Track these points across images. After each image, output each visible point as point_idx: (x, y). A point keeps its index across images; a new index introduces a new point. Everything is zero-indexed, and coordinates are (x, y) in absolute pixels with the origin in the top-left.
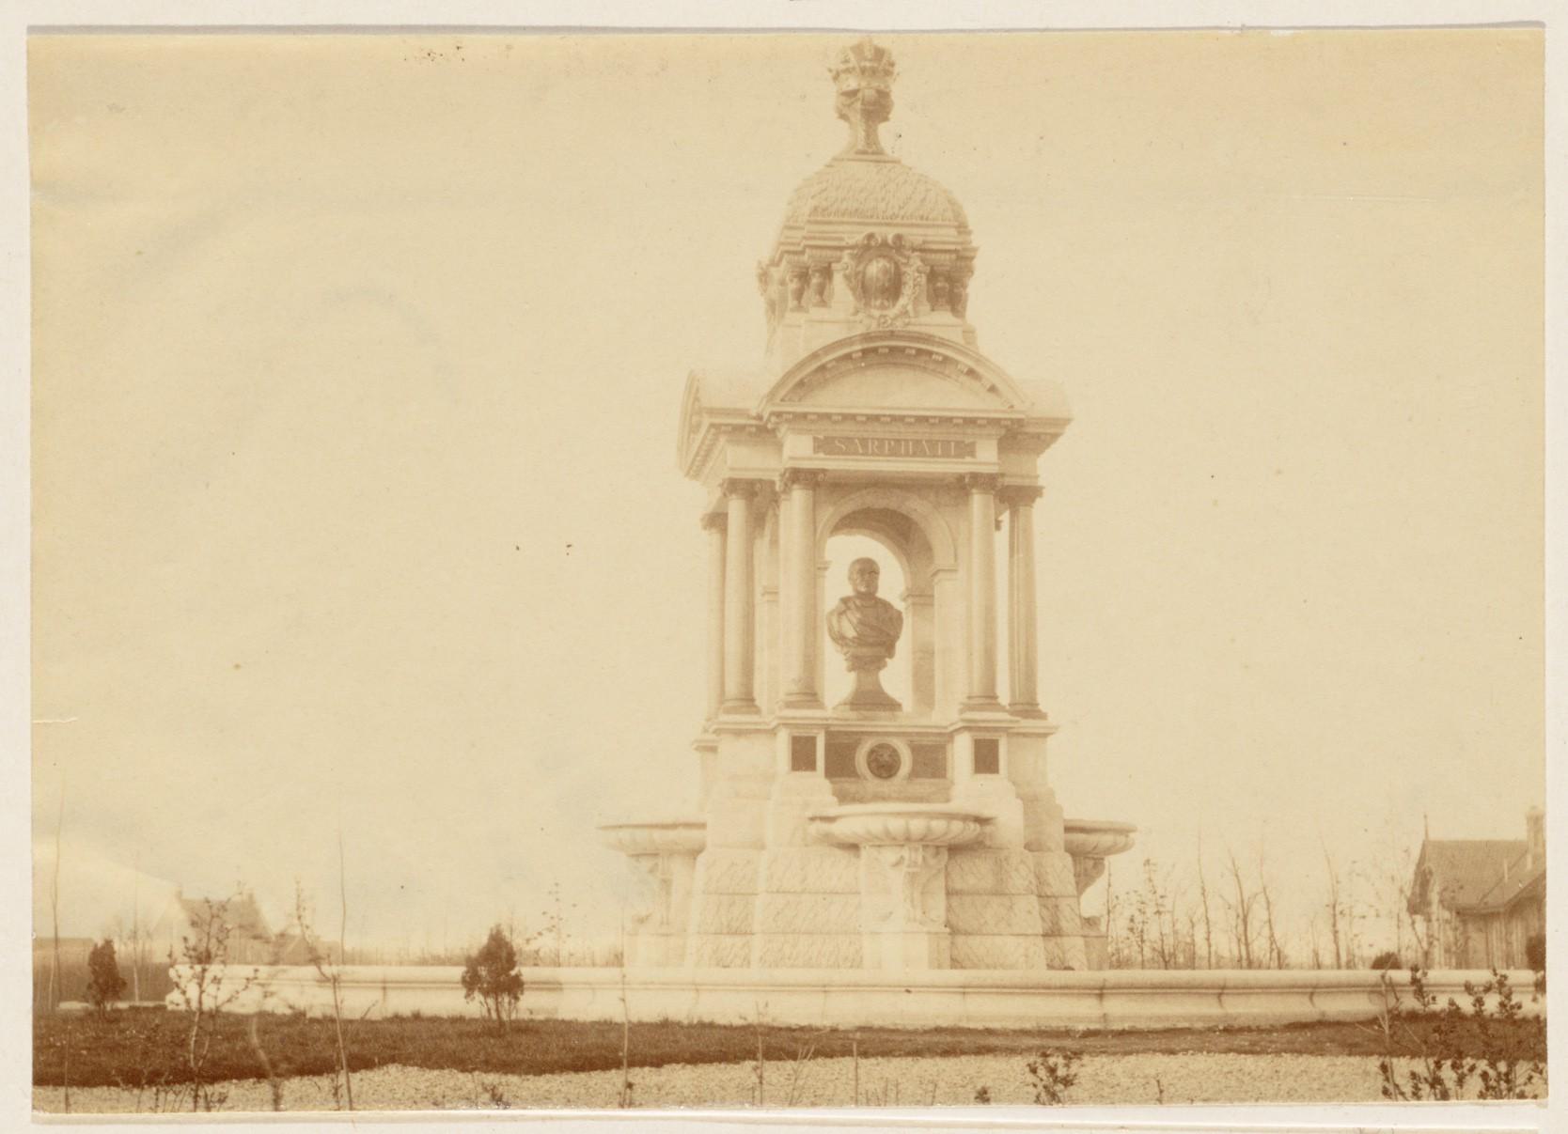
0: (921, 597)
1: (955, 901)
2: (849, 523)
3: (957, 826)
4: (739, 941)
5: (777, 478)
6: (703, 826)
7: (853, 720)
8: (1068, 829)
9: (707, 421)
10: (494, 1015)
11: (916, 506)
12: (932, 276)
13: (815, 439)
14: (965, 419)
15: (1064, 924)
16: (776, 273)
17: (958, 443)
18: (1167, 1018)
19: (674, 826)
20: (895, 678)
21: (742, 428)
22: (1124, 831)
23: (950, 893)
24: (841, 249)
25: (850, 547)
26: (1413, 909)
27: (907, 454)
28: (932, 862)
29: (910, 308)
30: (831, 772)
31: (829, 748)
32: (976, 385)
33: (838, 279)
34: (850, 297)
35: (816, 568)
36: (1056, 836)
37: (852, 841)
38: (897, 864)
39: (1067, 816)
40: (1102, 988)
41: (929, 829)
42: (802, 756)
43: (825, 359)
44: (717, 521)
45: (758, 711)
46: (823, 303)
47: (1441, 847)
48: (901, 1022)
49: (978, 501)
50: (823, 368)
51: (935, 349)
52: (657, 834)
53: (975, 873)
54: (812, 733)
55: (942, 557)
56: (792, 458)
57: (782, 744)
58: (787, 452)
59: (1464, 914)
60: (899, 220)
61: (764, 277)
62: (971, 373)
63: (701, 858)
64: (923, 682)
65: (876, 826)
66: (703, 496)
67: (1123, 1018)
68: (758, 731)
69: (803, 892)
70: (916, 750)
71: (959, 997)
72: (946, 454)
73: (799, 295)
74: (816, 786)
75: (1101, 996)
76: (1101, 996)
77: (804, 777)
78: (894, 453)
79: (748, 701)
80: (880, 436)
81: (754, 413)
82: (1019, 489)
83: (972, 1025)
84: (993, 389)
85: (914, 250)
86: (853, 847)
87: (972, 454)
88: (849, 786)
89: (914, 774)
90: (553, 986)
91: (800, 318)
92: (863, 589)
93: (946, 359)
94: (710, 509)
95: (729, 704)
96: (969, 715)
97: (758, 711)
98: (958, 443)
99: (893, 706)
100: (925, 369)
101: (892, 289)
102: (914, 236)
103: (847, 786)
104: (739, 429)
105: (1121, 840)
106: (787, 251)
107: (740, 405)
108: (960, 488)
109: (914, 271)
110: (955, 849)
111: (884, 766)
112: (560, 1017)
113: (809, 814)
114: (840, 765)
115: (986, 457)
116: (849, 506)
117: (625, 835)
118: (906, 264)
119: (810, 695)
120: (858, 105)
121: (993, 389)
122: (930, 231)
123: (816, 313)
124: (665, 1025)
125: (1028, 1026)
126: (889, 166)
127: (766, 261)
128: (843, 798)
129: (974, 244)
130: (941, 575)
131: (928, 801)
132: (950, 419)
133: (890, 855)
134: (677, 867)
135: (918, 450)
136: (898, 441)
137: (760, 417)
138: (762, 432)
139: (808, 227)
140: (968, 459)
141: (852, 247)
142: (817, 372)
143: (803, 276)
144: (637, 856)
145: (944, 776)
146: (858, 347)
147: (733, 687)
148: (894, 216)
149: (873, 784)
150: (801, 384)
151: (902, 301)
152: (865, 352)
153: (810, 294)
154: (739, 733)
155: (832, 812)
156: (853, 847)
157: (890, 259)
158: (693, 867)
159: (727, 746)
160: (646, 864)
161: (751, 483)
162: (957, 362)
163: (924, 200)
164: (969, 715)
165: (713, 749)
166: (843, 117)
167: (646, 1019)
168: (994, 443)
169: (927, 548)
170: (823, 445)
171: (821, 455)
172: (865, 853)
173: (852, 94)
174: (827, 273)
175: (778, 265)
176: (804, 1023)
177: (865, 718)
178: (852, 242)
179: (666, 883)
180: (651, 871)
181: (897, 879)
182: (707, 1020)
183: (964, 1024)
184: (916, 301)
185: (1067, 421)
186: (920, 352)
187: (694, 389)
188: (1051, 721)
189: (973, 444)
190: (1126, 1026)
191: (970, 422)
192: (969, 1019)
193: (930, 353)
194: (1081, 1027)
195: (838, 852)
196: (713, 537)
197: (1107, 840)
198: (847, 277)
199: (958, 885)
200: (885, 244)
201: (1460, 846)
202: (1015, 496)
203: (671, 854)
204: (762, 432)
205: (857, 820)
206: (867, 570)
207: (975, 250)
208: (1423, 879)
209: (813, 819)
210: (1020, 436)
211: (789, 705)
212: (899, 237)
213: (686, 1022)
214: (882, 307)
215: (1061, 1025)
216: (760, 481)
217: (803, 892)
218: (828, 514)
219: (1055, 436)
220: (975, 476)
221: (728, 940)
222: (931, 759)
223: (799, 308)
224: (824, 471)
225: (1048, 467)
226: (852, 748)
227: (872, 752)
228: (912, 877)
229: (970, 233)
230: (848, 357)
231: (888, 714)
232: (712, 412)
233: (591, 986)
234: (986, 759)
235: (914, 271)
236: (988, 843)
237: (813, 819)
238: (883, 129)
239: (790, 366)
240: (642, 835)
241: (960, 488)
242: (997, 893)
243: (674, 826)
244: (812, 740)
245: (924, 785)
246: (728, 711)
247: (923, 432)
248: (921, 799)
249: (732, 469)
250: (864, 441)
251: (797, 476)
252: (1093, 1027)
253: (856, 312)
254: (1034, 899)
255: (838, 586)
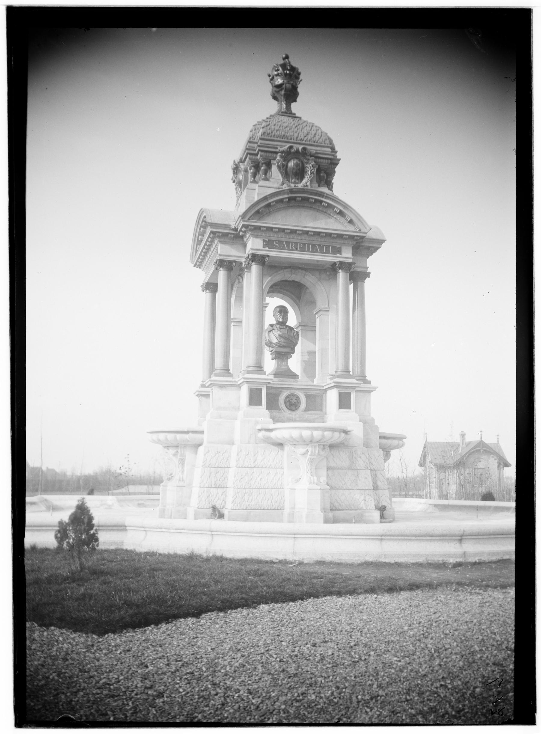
0: (308, 326)
1: (330, 473)
2: (276, 288)
3: (327, 434)
4: (220, 491)
5: (243, 261)
6: (202, 432)
7: (276, 382)
8: (380, 437)
9: (209, 230)
10: (216, 242)
11: (308, 279)
12: (319, 171)
13: (264, 241)
14: (338, 235)
15: (379, 483)
16: (242, 166)
17: (333, 247)
18: (498, 553)
19: (187, 432)
20: (294, 363)
21: (226, 235)
22: (401, 438)
23: (328, 468)
24: (276, 153)
25: (275, 302)
26: (421, 465)
27: (309, 251)
28: (322, 453)
29: (308, 184)
30: (268, 408)
31: (268, 394)
32: (342, 219)
33: (274, 168)
34: (280, 177)
35: (262, 307)
36: (375, 441)
37: (280, 442)
38: (305, 454)
39: (380, 431)
40: (462, 536)
41: (323, 436)
42: (254, 398)
43: (270, 201)
44: (211, 287)
45: (231, 376)
46: (266, 179)
47: (432, 444)
48: (346, 559)
49: (341, 276)
50: (269, 205)
51: (324, 200)
52: (178, 436)
53: (341, 459)
54: (259, 387)
55: (321, 303)
56: (252, 249)
57: (245, 391)
58: (249, 246)
59: (441, 468)
60: (304, 142)
61: (236, 170)
62: (341, 213)
63: (201, 449)
64: (309, 366)
65: (295, 434)
66: (202, 276)
67: (475, 554)
68: (232, 385)
69: (254, 467)
70: (308, 397)
71: (378, 542)
72: (327, 252)
73: (254, 175)
74: (262, 411)
75: (460, 541)
76: (460, 541)
77: (255, 409)
78: (303, 249)
79: (226, 371)
80: (296, 241)
81: (233, 227)
82: (358, 273)
83: (387, 561)
84: (351, 222)
85: (311, 156)
86: (280, 445)
87: (340, 252)
88: (276, 414)
89: (307, 409)
90: (121, 528)
91: (255, 186)
92: (281, 320)
93: (329, 206)
94: (206, 281)
95: (216, 372)
96: (336, 380)
97: (231, 376)
98: (333, 247)
99: (295, 376)
100: (318, 210)
101: (300, 174)
102: (312, 149)
103: (275, 414)
104: (225, 235)
105: (401, 442)
106: (249, 152)
107: (226, 223)
108: (332, 270)
109: (310, 167)
110: (332, 446)
111: (292, 404)
112: (125, 548)
113: (259, 427)
114: (272, 405)
115: (347, 255)
116: (278, 277)
117: (162, 436)
118: (307, 163)
119: (259, 368)
120: (283, 92)
121: (351, 222)
122: (318, 148)
123: (262, 183)
124: (191, 557)
125: (421, 560)
126: (298, 119)
127: (237, 160)
128: (275, 420)
129: (338, 157)
130: (321, 313)
131: (314, 422)
132: (330, 234)
133: (301, 450)
134: (189, 454)
135: (314, 249)
136: (304, 244)
137: (236, 229)
138: (235, 237)
139: (260, 141)
140: (338, 255)
141: (282, 152)
142: (262, 209)
143: (256, 166)
144: (168, 447)
145: (321, 410)
146: (286, 196)
147: (219, 363)
148: (301, 140)
149: (287, 413)
150: (258, 212)
151: (305, 181)
152: (290, 199)
153: (261, 175)
154: (221, 386)
155: (272, 426)
156: (280, 445)
157: (300, 160)
158: (196, 453)
159: (216, 392)
160: (172, 451)
161: (230, 262)
162: (334, 207)
163: (315, 134)
164: (336, 380)
165: (207, 396)
166: (275, 98)
167: (179, 552)
168: (351, 248)
169: (313, 303)
170: (268, 244)
171: (267, 249)
172: (287, 448)
173: (279, 86)
174: (269, 165)
175: (243, 162)
176: (281, 557)
177: (282, 381)
178: (282, 149)
179: (182, 461)
180: (174, 455)
181: (304, 463)
182: (218, 554)
183: (383, 560)
184: (311, 182)
185: (383, 241)
186: (317, 201)
187: (202, 211)
188: (373, 384)
189: (340, 248)
190: (476, 559)
191: (340, 236)
192: (385, 556)
193: (321, 202)
194: (452, 561)
195: (272, 447)
196: (207, 295)
197: (395, 442)
198: (279, 167)
199: (332, 464)
200: (297, 151)
201: (437, 443)
202: (358, 277)
203: (185, 446)
204: (235, 237)
205: (285, 430)
206: (283, 311)
207: (339, 160)
208: (424, 456)
209: (260, 430)
210: (365, 246)
211: (248, 372)
212: (304, 149)
213: (205, 555)
214: (295, 183)
215: (441, 559)
216: (235, 262)
217: (254, 467)
218: (268, 281)
219: (376, 249)
220: (341, 263)
221: (214, 491)
222: (315, 401)
223: (254, 182)
224: (268, 256)
225: (373, 263)
226: (277, 395)
227: (287, 397)
228: (312, 461)
229: (336, 152)
230: (281, 201)
231: (292, 380)
232: (212, 225)
233: (144, 529)
234: (344, 402)
235: (310, 167)
236: (346, 443)
237: (260, 430)
238: (293, 105)
239: (249, 205)
240: (170, 436)
241: (332, 270)
242: (350, 468)
243: (187, 432)
244: (261, 390)
245: (311, 415)
246: (216, 375)
247: (317, 241)
248: (310, 421)
249: (220, 255)
250: (288, 243)
251: (254, 258)
252: (458, 560)
253: (283, 184)
254: (368, 472)
255: (270, 318)
